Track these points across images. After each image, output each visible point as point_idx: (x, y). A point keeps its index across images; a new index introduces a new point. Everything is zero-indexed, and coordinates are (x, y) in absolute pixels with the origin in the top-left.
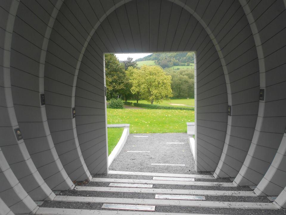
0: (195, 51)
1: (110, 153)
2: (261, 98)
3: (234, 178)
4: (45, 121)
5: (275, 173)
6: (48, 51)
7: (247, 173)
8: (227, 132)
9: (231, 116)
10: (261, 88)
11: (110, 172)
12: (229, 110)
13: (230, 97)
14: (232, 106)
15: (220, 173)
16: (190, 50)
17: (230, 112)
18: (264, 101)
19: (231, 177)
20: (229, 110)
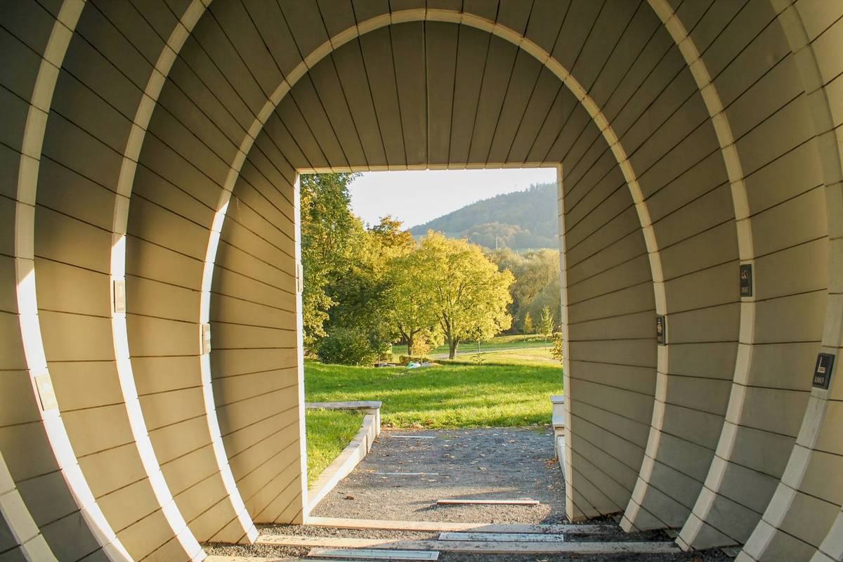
0: (560, 166)
1: (125, 559)
2: (745, 290)
3: (679, 529)
4: (631, 181)
5: (773, 537)
6: (159, 103)
7: (727, 478)
8: (656, 395)
9: (665, 345)
10: (742, 263)
11: (308, 520)
12: (659, 328)
13: (659, 290)
14: (666, 317)
15: (638, 517)
16: (544, 160)
17: (662, 334)
18: (752, 299)
19: (670, 528)
20: (659, 328)
